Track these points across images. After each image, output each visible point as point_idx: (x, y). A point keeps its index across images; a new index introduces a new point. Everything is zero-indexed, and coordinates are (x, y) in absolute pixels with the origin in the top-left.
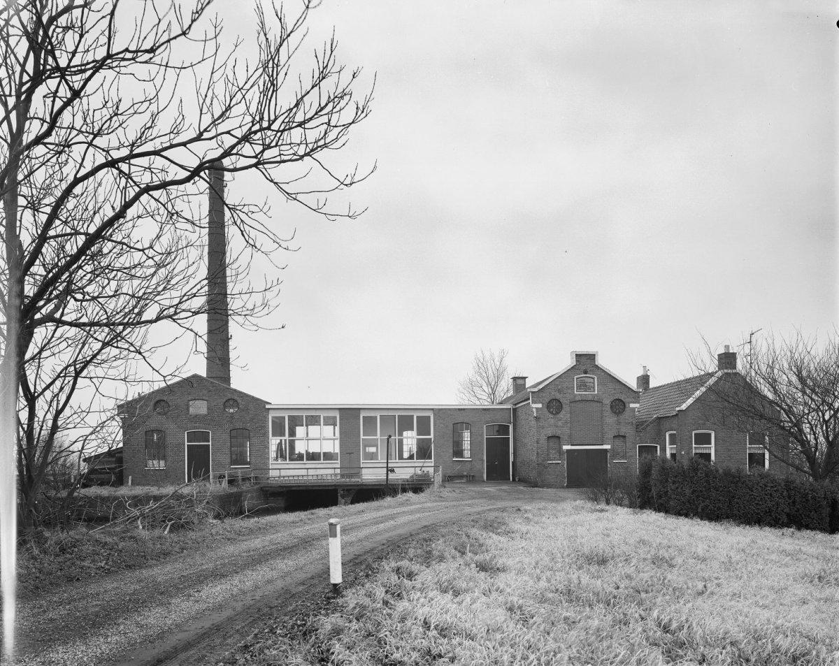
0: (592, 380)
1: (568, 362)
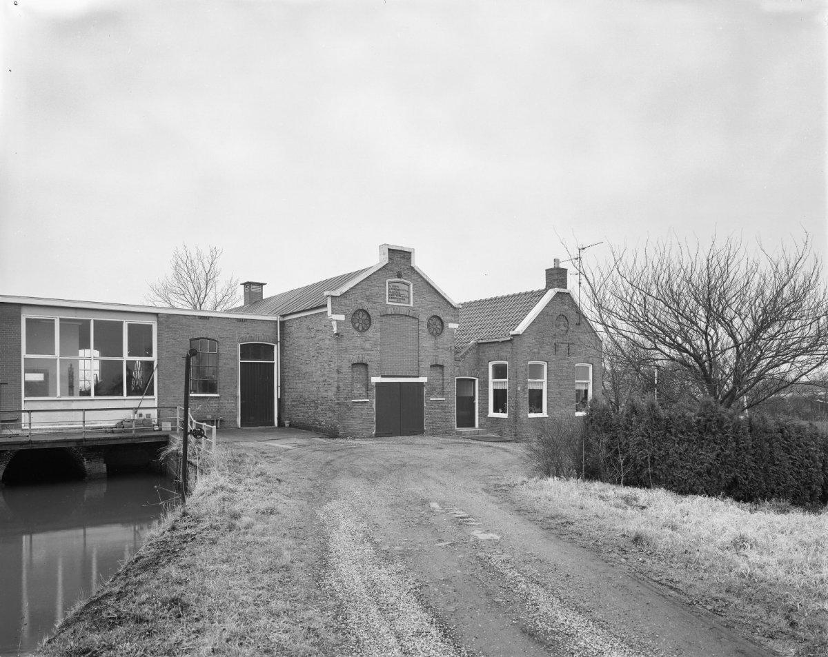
0: (406, 287)
1: (375, 260)
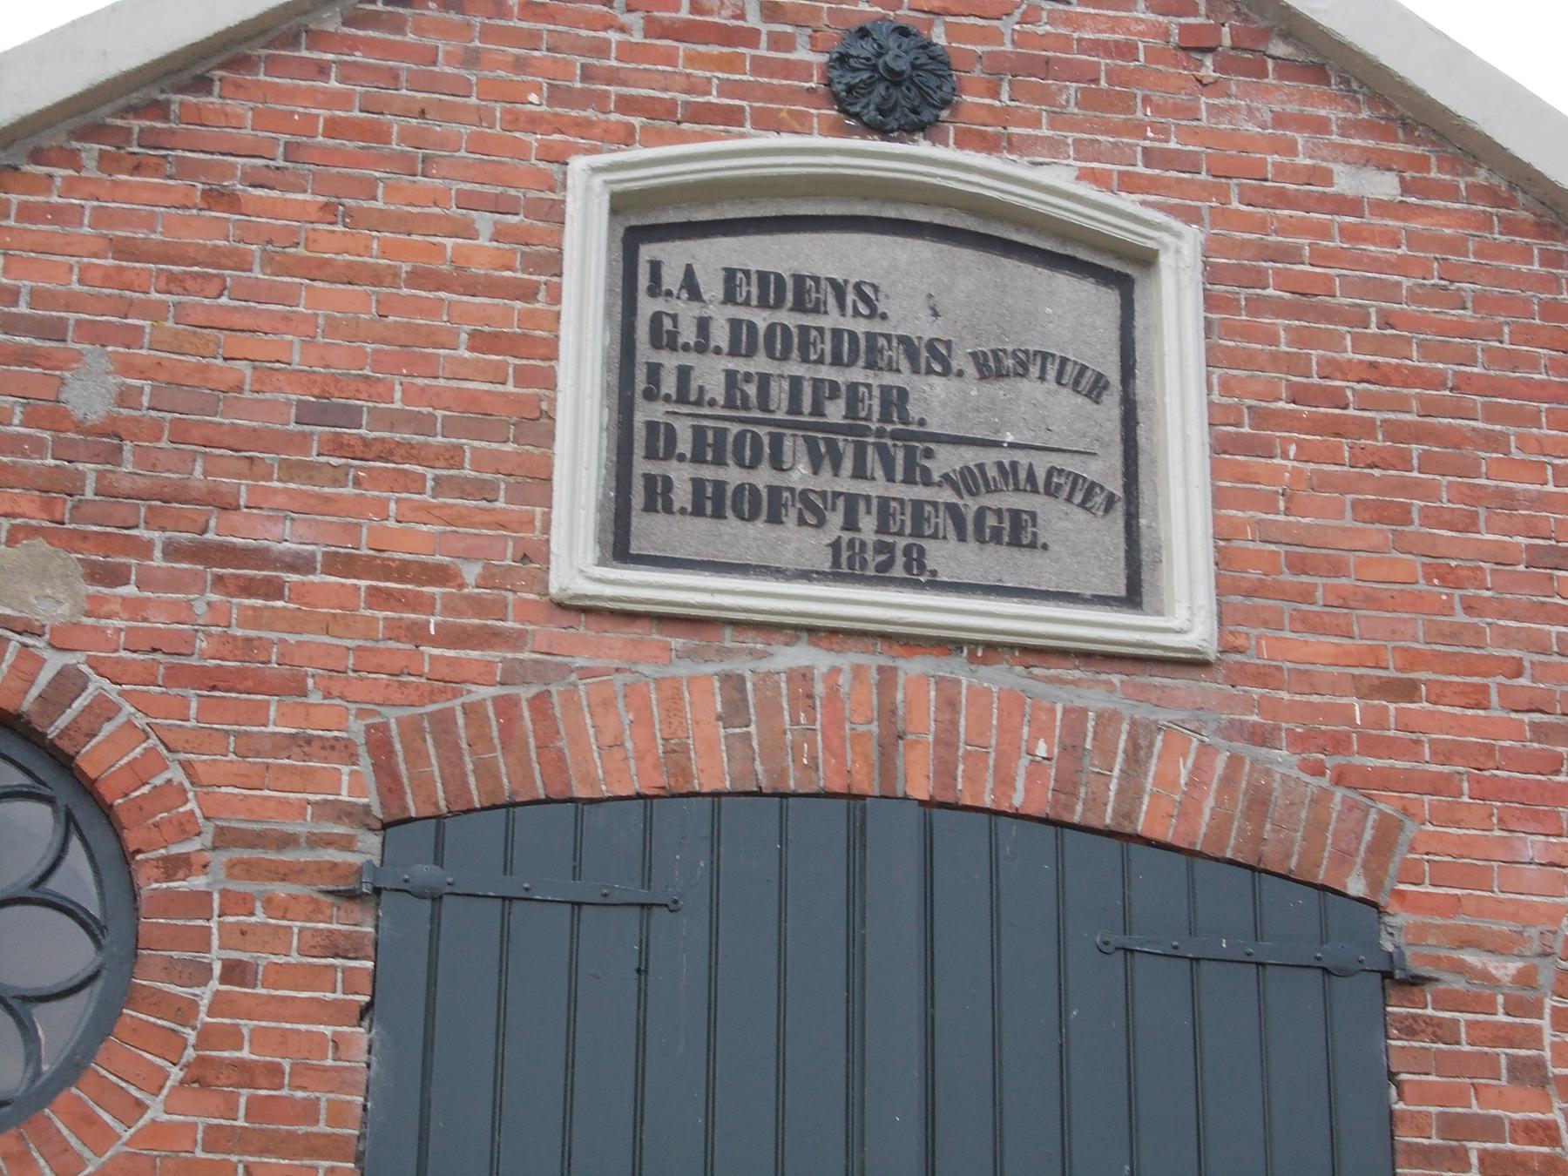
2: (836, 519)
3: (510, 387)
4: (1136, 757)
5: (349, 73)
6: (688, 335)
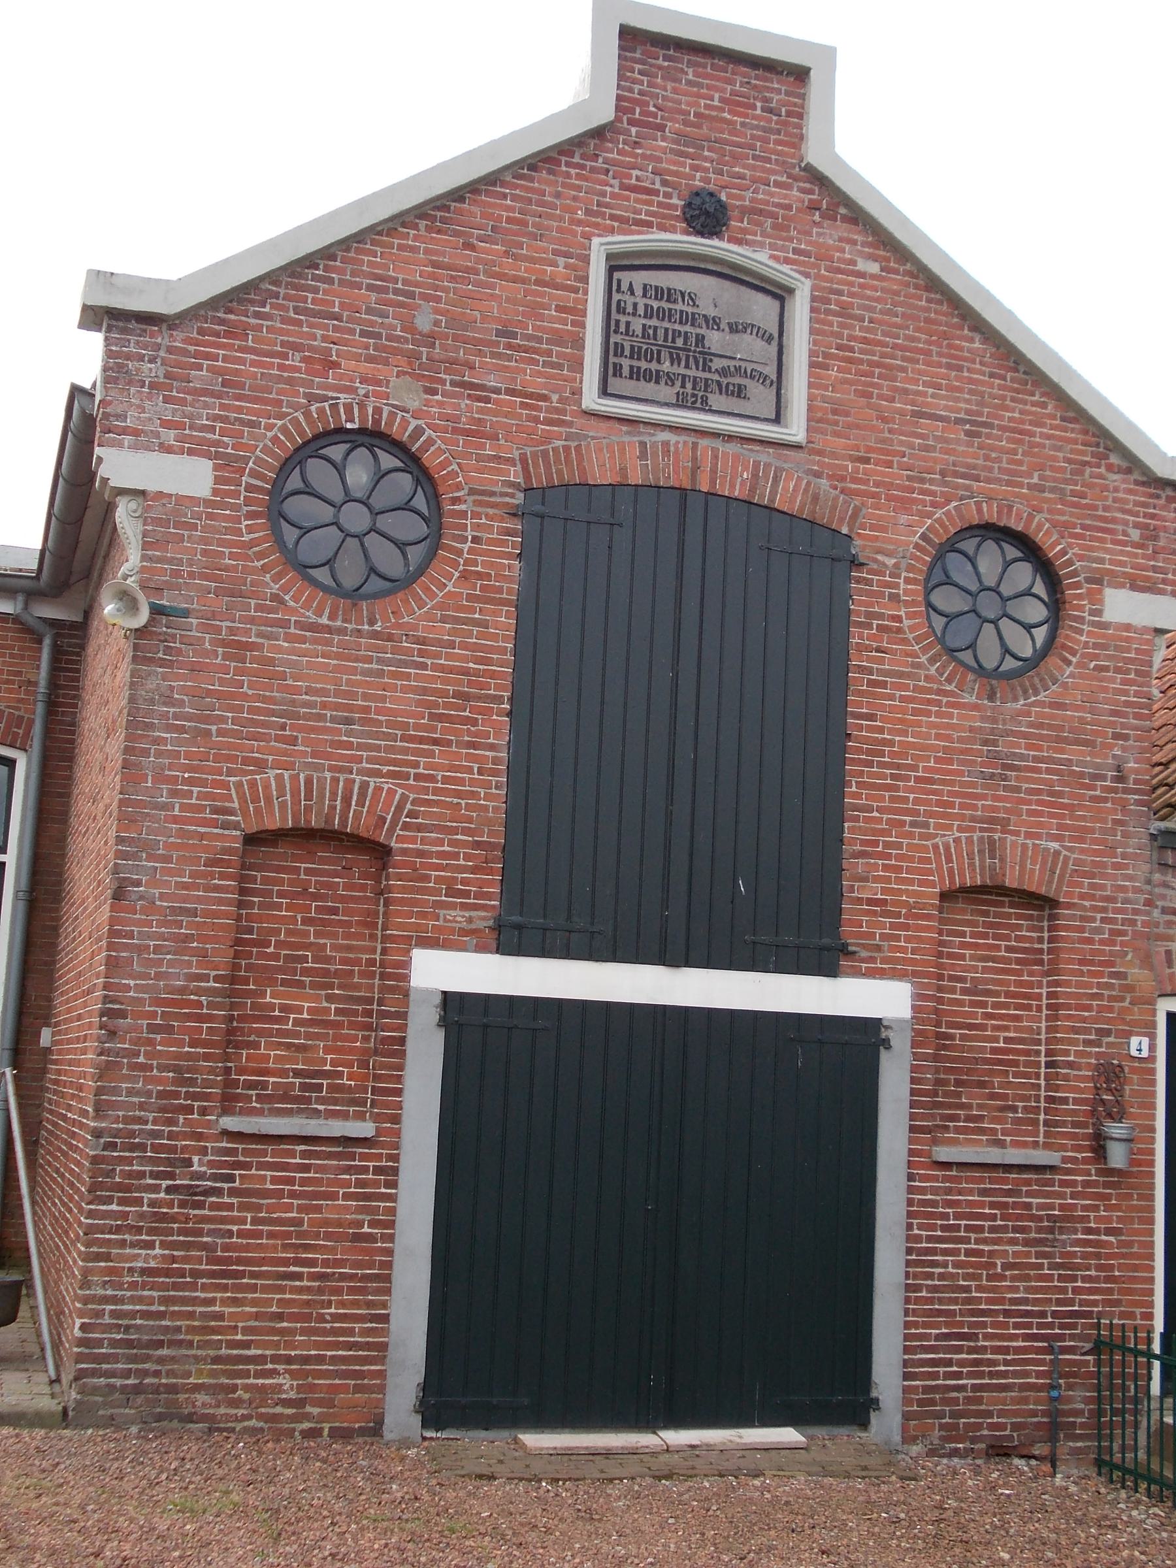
0: (762, 309)
2: (678, 383)
3: (569, 327)
4: (776, 480)
5: (514, 198)
6: (630, 309)
